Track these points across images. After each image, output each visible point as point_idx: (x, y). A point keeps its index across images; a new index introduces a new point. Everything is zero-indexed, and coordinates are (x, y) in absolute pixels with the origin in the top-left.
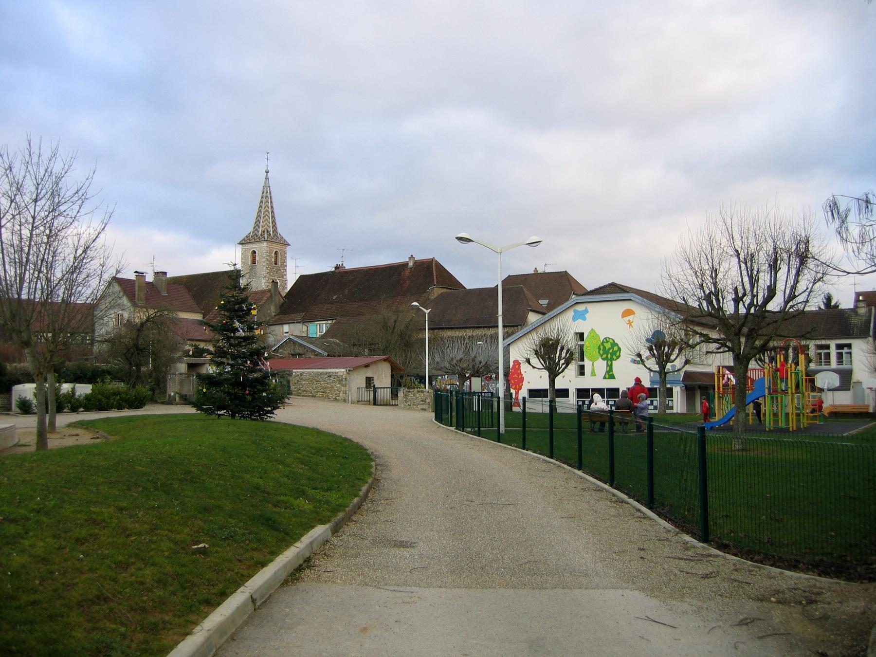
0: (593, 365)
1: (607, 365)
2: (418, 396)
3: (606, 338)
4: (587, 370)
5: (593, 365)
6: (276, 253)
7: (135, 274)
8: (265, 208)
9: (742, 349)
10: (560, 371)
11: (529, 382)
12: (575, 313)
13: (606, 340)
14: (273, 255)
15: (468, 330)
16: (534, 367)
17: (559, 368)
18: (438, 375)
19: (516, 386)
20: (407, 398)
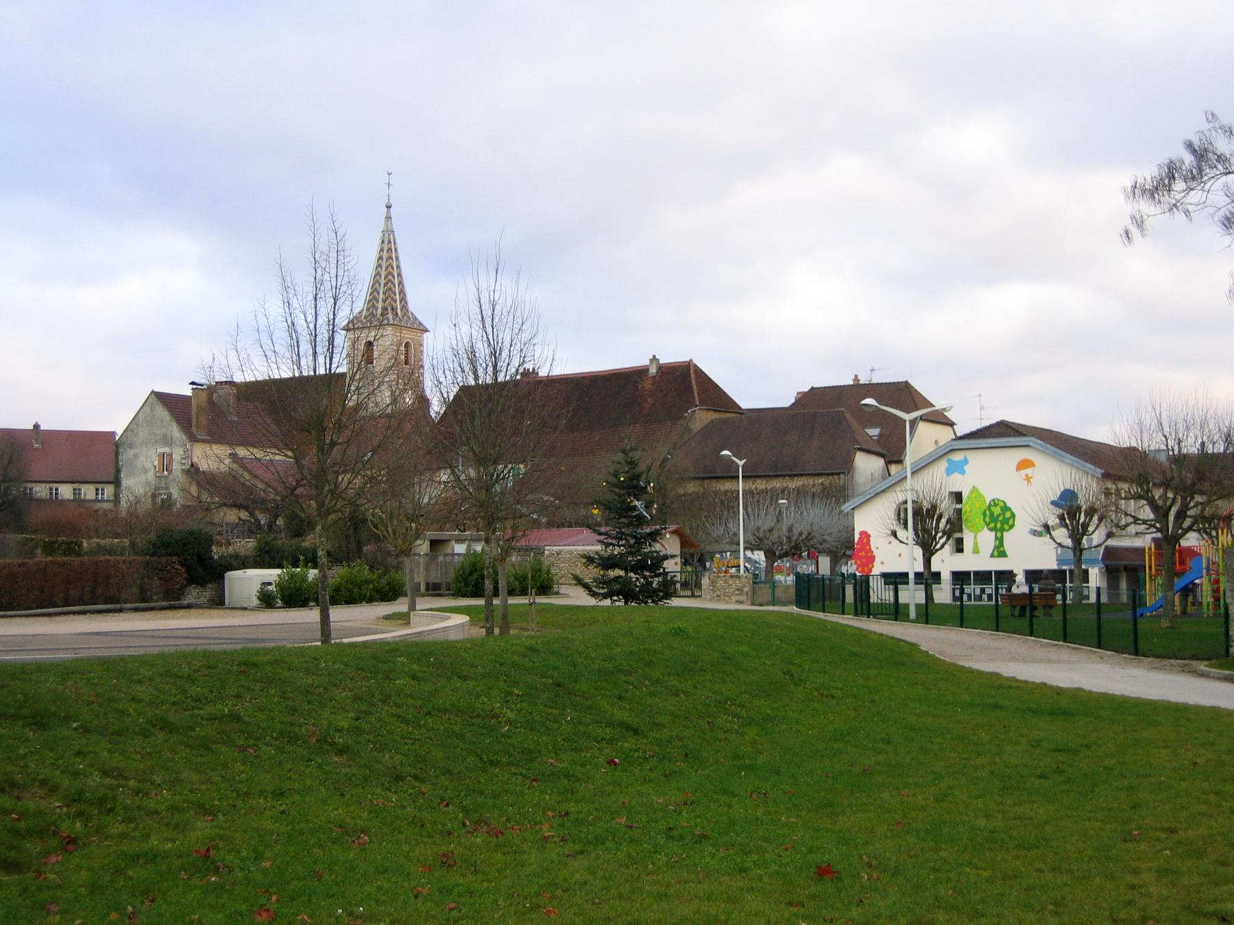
0: (975, 537)
1: (996, 538)
2: (731, 582)
3: (993, 500)
4: (968, 544)
5: (975, 537)
6: (407, 345)
7: (191, 386)
8: (387, 268)
9: (1170, 530)
10: (938, 547)
11: (882, 563)
12: (949, 464)
13: (995, 503)
14: (402, 348)
15: (759, 481)
16: (901, 542)
17: (936, 544)
18: (715, 553)
19: (863, 569)
20: (714, 586)
